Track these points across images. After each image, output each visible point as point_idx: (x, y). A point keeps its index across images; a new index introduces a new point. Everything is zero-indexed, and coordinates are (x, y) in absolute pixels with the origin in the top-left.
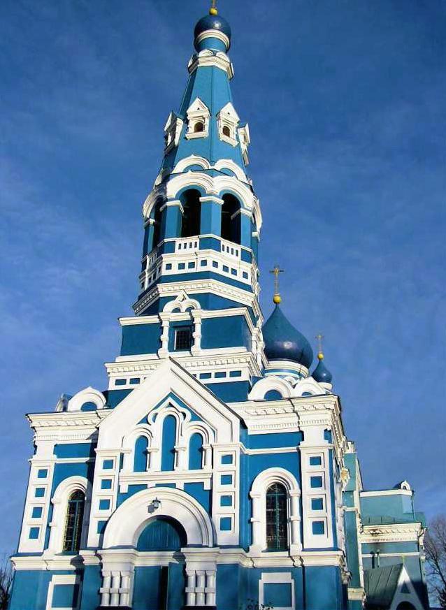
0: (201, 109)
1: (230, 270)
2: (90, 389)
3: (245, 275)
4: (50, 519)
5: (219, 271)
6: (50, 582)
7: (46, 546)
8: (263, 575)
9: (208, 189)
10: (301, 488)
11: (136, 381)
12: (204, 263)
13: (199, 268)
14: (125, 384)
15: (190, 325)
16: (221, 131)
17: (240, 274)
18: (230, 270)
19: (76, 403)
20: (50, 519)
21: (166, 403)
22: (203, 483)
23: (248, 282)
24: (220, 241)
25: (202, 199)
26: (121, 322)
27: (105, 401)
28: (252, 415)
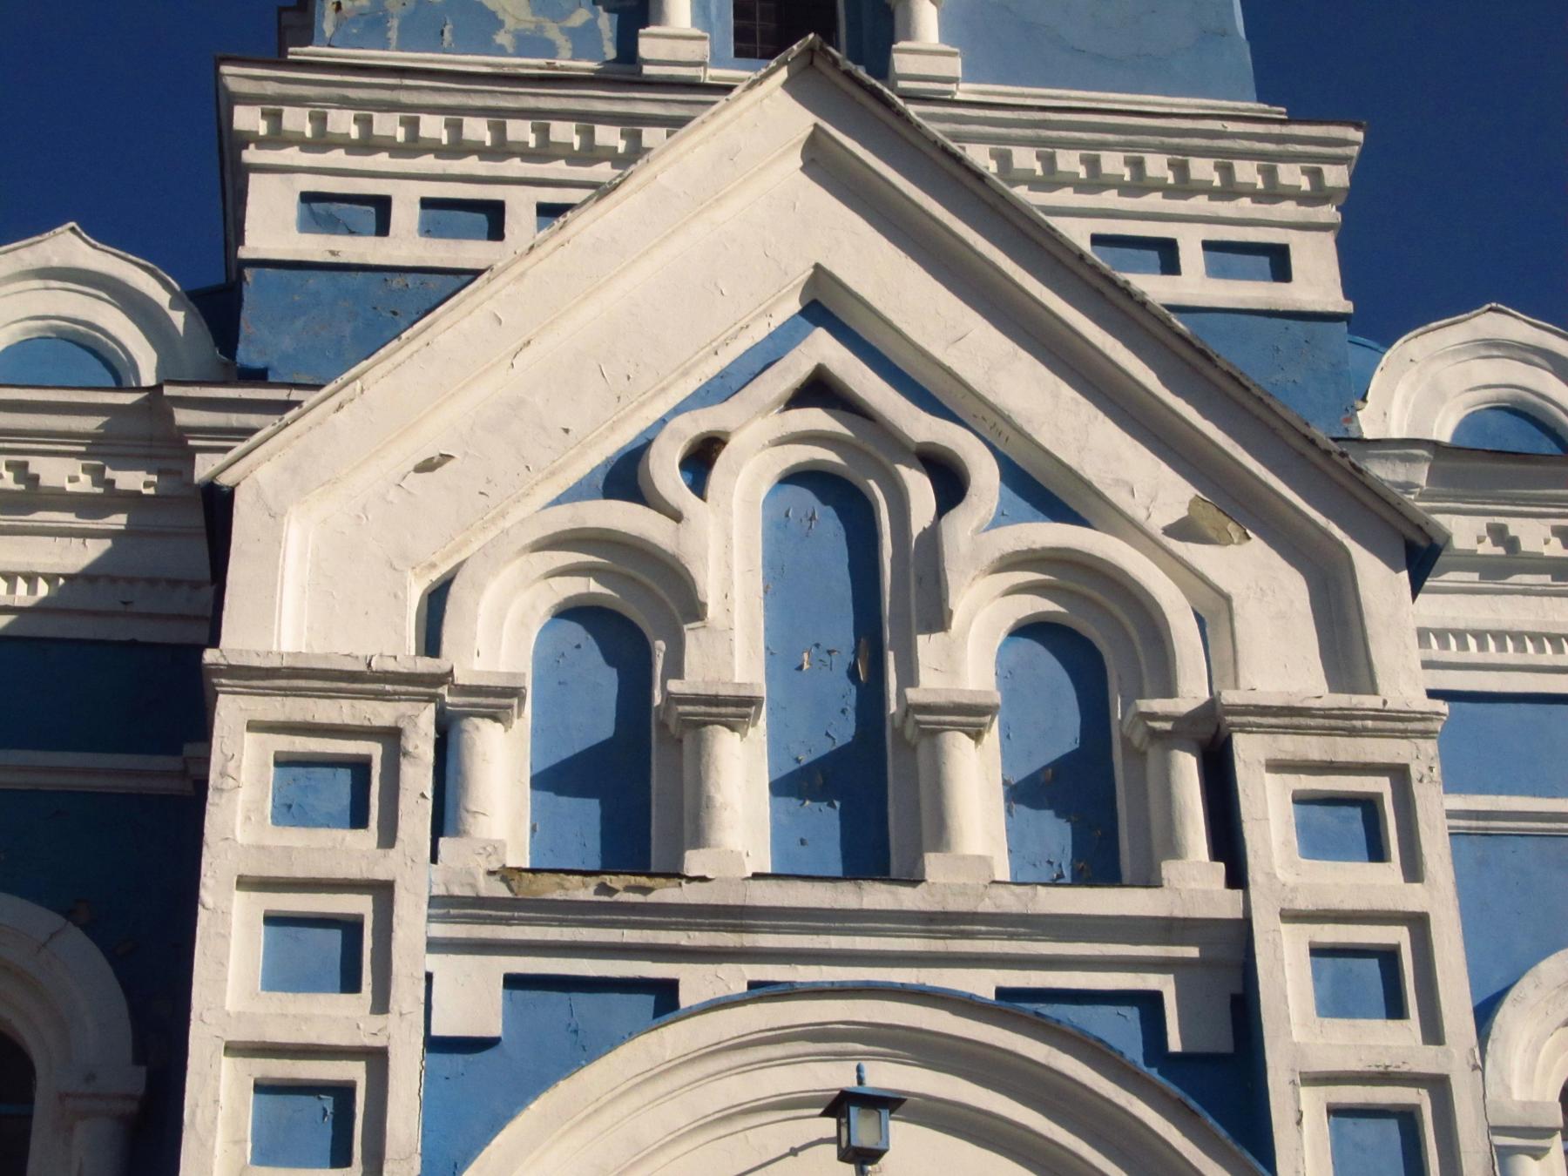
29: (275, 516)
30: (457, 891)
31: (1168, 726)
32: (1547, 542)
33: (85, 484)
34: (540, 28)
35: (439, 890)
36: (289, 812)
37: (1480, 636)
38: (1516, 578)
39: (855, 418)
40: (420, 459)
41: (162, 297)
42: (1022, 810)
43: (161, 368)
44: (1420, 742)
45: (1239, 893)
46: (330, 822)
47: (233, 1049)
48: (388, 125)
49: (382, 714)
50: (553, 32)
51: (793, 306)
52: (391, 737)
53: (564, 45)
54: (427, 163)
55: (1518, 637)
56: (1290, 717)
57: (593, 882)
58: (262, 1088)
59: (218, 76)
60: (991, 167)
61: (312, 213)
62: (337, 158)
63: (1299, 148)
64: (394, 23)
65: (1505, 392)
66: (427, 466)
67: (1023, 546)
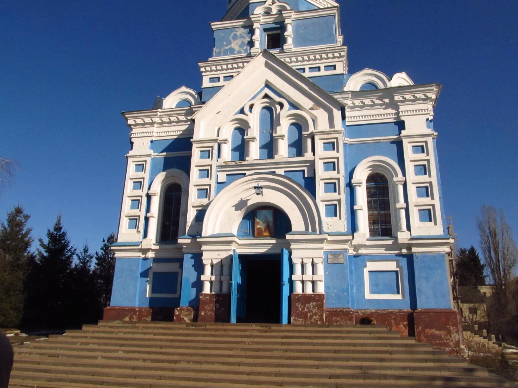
2: (184, 89)
4: (148, 210)
7: (145, 236)
8: (368, 264)
15: (281, 26)
21: (263, 94)
26: (213, 27)
29: (200, 122)
30: (220, 165)
31: (306, 135)
32: (369, 102)
33: (185, 119)
34: (240, 50)
35: (217, 165)
36: (202, 157)
37: (367, 116)
38: (365, 108)
39: (270, 99)
40: (217, 112)
41: (194, 94)
42: (290, 148)
43: (195, 103)
44: (340, 134)
45: (314, 156)
46: (207, 158)
47: (195, 186)
48: (219, 67)
49: (211, 144)
50: (242, 50)
51: (264, 85)
52: (212, 147)
53: (243, 52)
54: (224, 72)
55: (365, 116)
56: (322, 133)
57: (235, 162)
58: (198, 190)
59: (198, 65)
60: (283, 61)
61: (211, 80)
62: (213, 73)
63: (337, 50)
64: (222, 53)
65: (367, 81)
66: (218, 113)
67: (290, 114)
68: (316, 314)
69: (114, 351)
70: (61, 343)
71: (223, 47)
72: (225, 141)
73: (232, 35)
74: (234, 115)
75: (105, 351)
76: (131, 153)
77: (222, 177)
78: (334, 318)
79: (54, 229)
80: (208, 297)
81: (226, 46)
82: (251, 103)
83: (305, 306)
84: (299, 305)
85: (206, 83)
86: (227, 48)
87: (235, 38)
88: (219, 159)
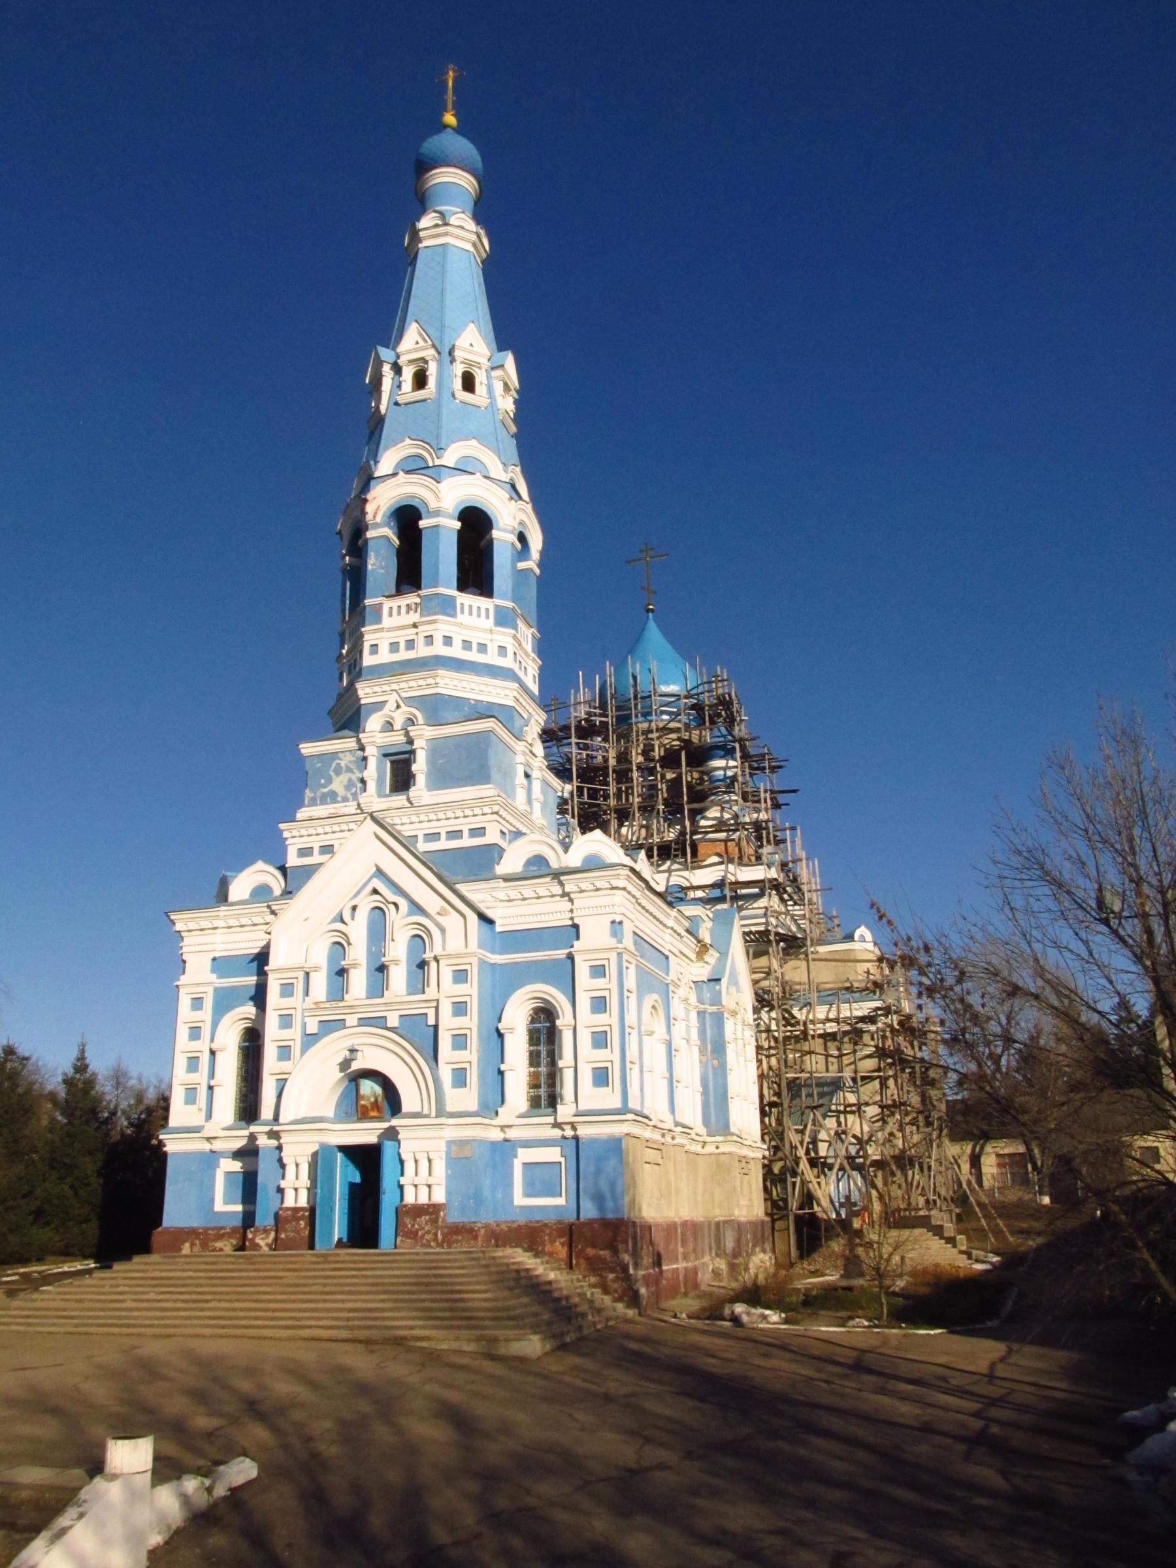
0: (422, 343)
1: (475, 647)
2: (260, 865)
3: (502, 650)
4: (212, 1074)
5: (456, 652)
6: (218, 1170)
7: (209, 1116)
8: (521, 1151)
9: (433, 504)
10: (575, 1017)
11: (328, 849)
12: (429, 639)
13: (422, 651)
14: (311, 854)
16: (458, 384)
17: (492, 649)
18: (475, 647)
19: (241, 886)
20: (212, 1074)
21: (369, 888)
22: (426, 1014)
23: (507, 662)
24: (453, 598)
25: (422, 524)
26: (303, 751)
27: (283, 885)
28: (501, 901)
68: (428, 1232)
69: (142, 1293)
70: (87, 1286)
71: (319, 789)
72: (316, 969)
73: (334, 765)
74: (330, 923)
75: (136, 1293)
76: (183, 980)
77: (312, 1028)
78: (455, 1237)
79: (75, 1069)
80: (289, 1212)
81: (325, 786)
82: (353, 903)
83: (415, 1220)
84: (408, 1221)
85: (293, 860)
86: (325, 790)
87: (338, 771)
88: (307, 998)
